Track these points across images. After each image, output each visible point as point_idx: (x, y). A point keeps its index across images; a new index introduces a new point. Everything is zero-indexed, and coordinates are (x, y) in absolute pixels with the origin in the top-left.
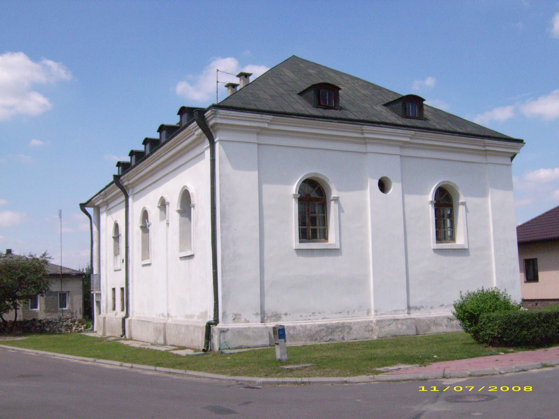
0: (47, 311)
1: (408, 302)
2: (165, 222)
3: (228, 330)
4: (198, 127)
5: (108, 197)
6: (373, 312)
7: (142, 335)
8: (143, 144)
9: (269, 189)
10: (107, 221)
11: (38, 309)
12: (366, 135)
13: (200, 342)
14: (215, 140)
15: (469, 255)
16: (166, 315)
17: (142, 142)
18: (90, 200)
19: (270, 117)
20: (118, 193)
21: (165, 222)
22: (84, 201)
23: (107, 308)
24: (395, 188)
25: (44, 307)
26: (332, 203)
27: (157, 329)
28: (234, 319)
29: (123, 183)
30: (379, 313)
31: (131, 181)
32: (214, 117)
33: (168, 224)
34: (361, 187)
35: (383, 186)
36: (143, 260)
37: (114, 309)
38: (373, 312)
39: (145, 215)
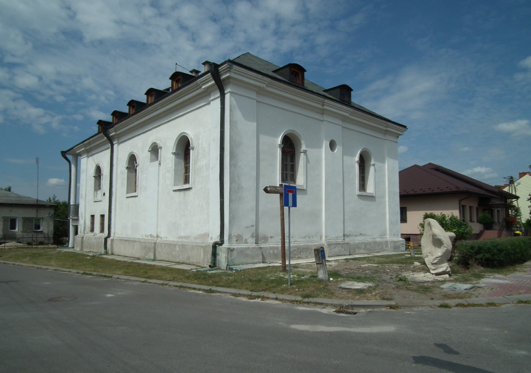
0: (23, 232)
1: (344, 231)
2: (158, 162)
3: (234, 249)
4: (212, 78)
5: (92, 146)
6: (324, 238)
7: (121, 251)
8: (128, 105)
9: (263, 138)
10: (87, 165)
11: (17, 230)
12: (325, 107)
13: (205, 260)
14: (226, 92)
15: (375, 200)
16: (155, 236)
17: (127, 103)
18: (72, 148)
19: (269, 80)
20: (105, 141)
21: (158, 162)
22: (65, 150)
23: (85, 229)
24: (338, 149)
25: (21, 229)
26: (302, 154)
27: (145, 247)
28: (237, 241)
29: (110, 134)
30: (328, 238)
31: (118, 132)
32: (228, 71)
33: (160, 164)
34: (319, 146)
35: (332, 145)
36: (127, 193)
37: (92, 230)
38: (324, 238)
39: (132, 159)
